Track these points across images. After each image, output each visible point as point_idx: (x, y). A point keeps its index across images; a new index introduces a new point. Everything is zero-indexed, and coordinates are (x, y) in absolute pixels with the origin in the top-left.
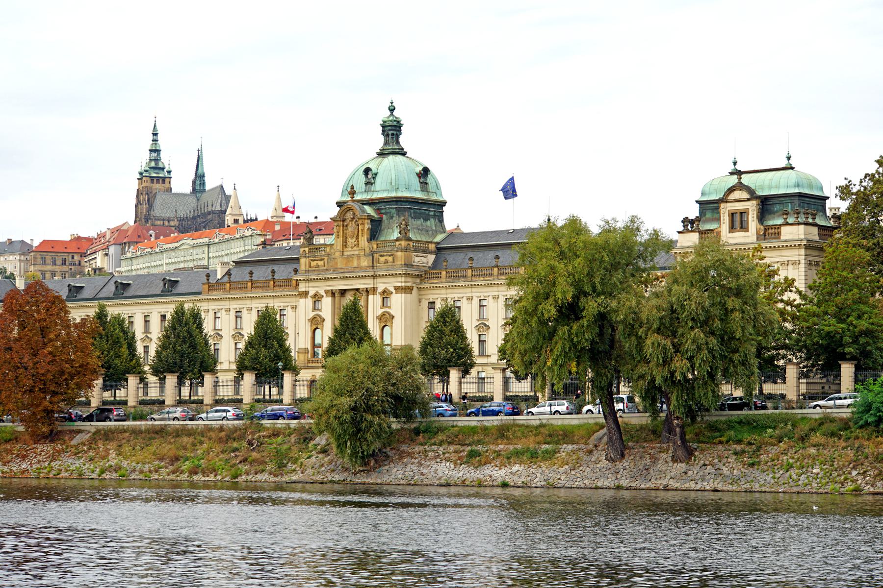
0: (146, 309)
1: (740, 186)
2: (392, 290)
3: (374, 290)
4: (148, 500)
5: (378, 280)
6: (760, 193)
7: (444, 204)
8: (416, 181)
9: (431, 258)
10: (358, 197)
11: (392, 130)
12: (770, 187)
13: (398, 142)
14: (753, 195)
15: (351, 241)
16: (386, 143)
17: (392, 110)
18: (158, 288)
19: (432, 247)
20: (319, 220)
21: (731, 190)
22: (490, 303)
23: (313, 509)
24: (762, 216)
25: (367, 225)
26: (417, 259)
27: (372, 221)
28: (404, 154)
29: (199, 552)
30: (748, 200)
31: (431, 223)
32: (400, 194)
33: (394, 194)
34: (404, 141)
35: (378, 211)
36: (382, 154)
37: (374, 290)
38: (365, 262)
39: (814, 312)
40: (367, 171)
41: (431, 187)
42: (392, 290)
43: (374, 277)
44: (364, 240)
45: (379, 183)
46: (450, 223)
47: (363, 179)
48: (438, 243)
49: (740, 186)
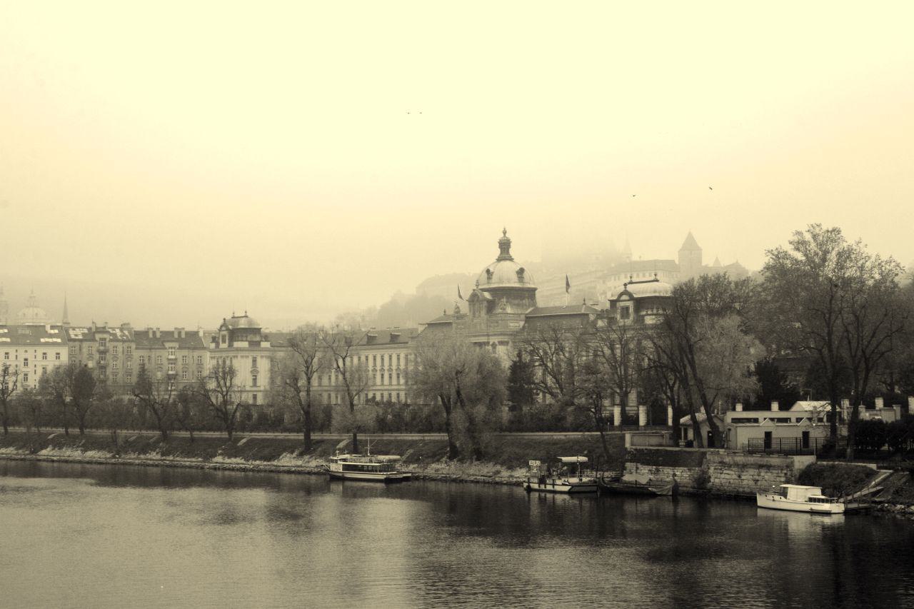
0: (382, 352)
1: (626, 292)
2: (497, 343)
4: (92, 485)
5: (491, 337)
6: (635, 296)
8: (514, 277)
9: (522, 323)
10: (480, 287)
11: (505, 245)
14: (631, 298)
15: (477, 314)
16: (501, 253)
17: (505, 233)
18: (388, 339)
20: (642, 259)
21: (621, 294)
22: (259, 360)
23: (787, 428)
24: (637, 310)
25: (485, 304)
26: (511, 324)
27: (488, 301)
30: (629, 300)
31: (526, 301)
32: (504, 285)
34: (512, 252)
36: (499, 260)
37: (488, 343)
38: (483, 327)
40: (488, 271)
42: (497, 343)
43: (488, 335)
44: (483, 313)
45: (495, 278)
46: (541, 302)
47: (486, 275)
48: (527, 314)
49: (626, 292)
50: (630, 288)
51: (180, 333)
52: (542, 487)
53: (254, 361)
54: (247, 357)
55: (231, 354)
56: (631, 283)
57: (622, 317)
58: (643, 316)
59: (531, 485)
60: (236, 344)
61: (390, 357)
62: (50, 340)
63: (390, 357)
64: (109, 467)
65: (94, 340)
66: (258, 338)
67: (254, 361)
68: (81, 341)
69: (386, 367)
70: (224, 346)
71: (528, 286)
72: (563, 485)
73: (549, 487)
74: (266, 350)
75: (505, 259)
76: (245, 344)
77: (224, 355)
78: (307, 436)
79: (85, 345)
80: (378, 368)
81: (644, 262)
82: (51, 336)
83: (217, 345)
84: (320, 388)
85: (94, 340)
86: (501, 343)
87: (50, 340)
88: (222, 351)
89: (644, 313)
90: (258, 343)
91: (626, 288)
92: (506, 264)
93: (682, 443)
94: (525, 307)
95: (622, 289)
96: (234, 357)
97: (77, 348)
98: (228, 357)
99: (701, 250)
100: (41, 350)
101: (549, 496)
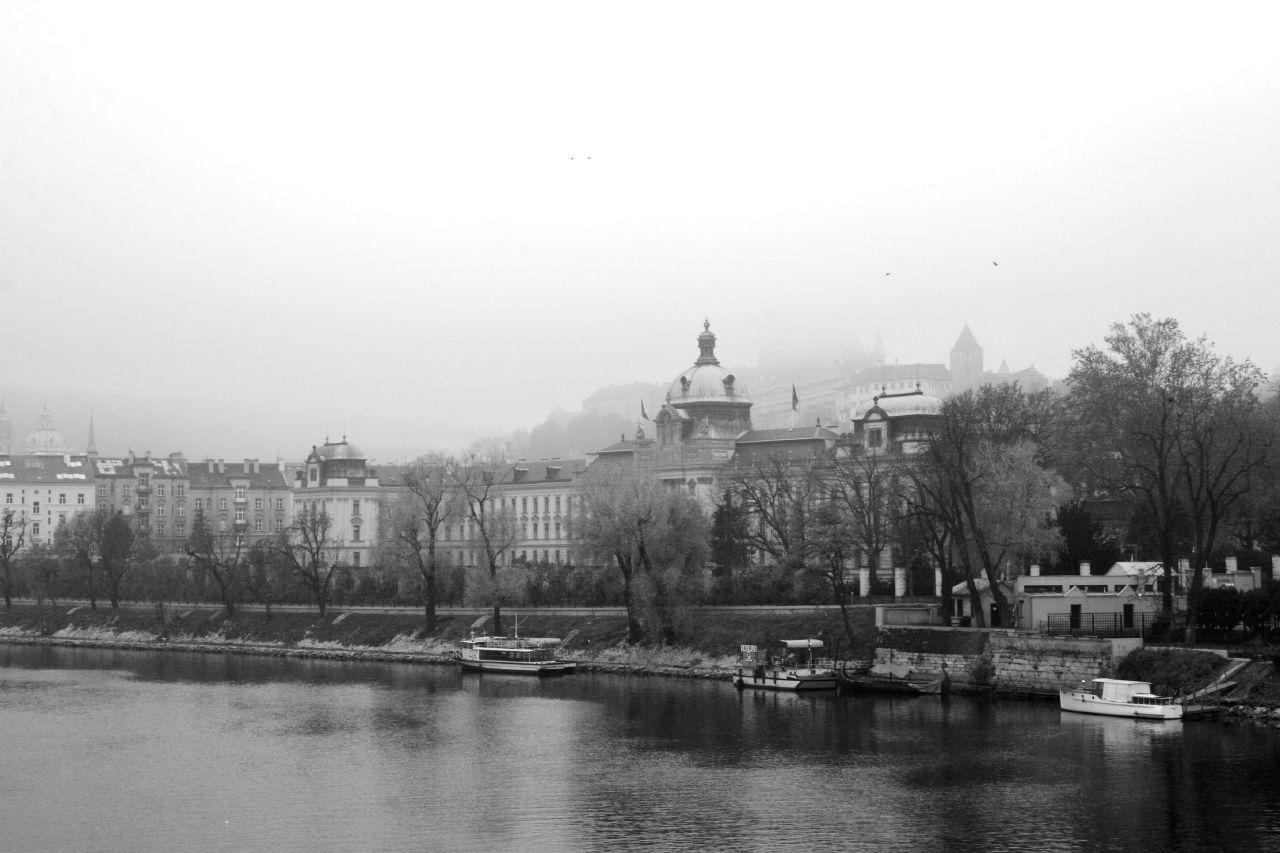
1: (876, 410)
2: (696, 481)
3: (684, 480)
5: (687, 473)
6: (889, 415)
7: (748, 406)
8: (721, 388)
9: (731, 453)
10: (672, 402)
11: (707, 344)
12: (900, 410)
13: (711, 353)
14: (884, 417)
15: (668, 440)
16: (702, 354)
17: (707, 326)
18: (544, 475)
19: (732, 444)
21: (870, 412)
22: (362, 504)
24: (892, 434)
25: (679, 425)
28: (716, 363)
29: (599, 799)
30: (880, 421)
31: (736, 422)
32: (706, 399)
33: (701, 400)
34: (717, 352)
35: (689, 413)
36: (699, 364)
38: (677, 457)
39: (1165, 492)
40: (683, 380)
41: (736, 392)
42: (696, 481)
43: (684, 470)
44: (677, 437)
45: (693, 389)
47: (681, 385)
49: (876, 410)
50: (883, 403)
51: (252, 467)
52: (760, 682)
53: (356, 505)
54: (346, 500)
55: (324, 496)
56: (884, 396)
57: (872, 444)
58: (901, 443)
59: (744, 679)
60: (331, 482)
61: (525, 500)
62: (70, 476)
63: (525, 500)
64: (152, 654)
65: (131, 476)
66: (361, 474)
67: (356, 505)
68: (113, 477)
69: (541, 515)
70: (313, 484)
71: (740, 400)
72: (789, 679)
73: (769, 683)
74: (372, 490)
75: (707, 363)
76: (343, 482)
77: (314, 497)
78: (430, 611)
79: (119, 483)
80: (530, 515)
81: (902, 367)
82: (72, 470)
83: (305, 484)
84: (448, 544)
85: (131, 476)
86: (702, 480)
87: (70, 476)
88: (311, 491)
89: (902, 438)
90: (362, 481)
91: (876, 403)
92: (708, 371)
93: (955, 620)
94: (735, 430)
95: (871, 404)
96: (328, 500)
97: (108, 488)
98: (319, 500)
99: (982, 350)
100: (57, 491)
101: (769, 694)
